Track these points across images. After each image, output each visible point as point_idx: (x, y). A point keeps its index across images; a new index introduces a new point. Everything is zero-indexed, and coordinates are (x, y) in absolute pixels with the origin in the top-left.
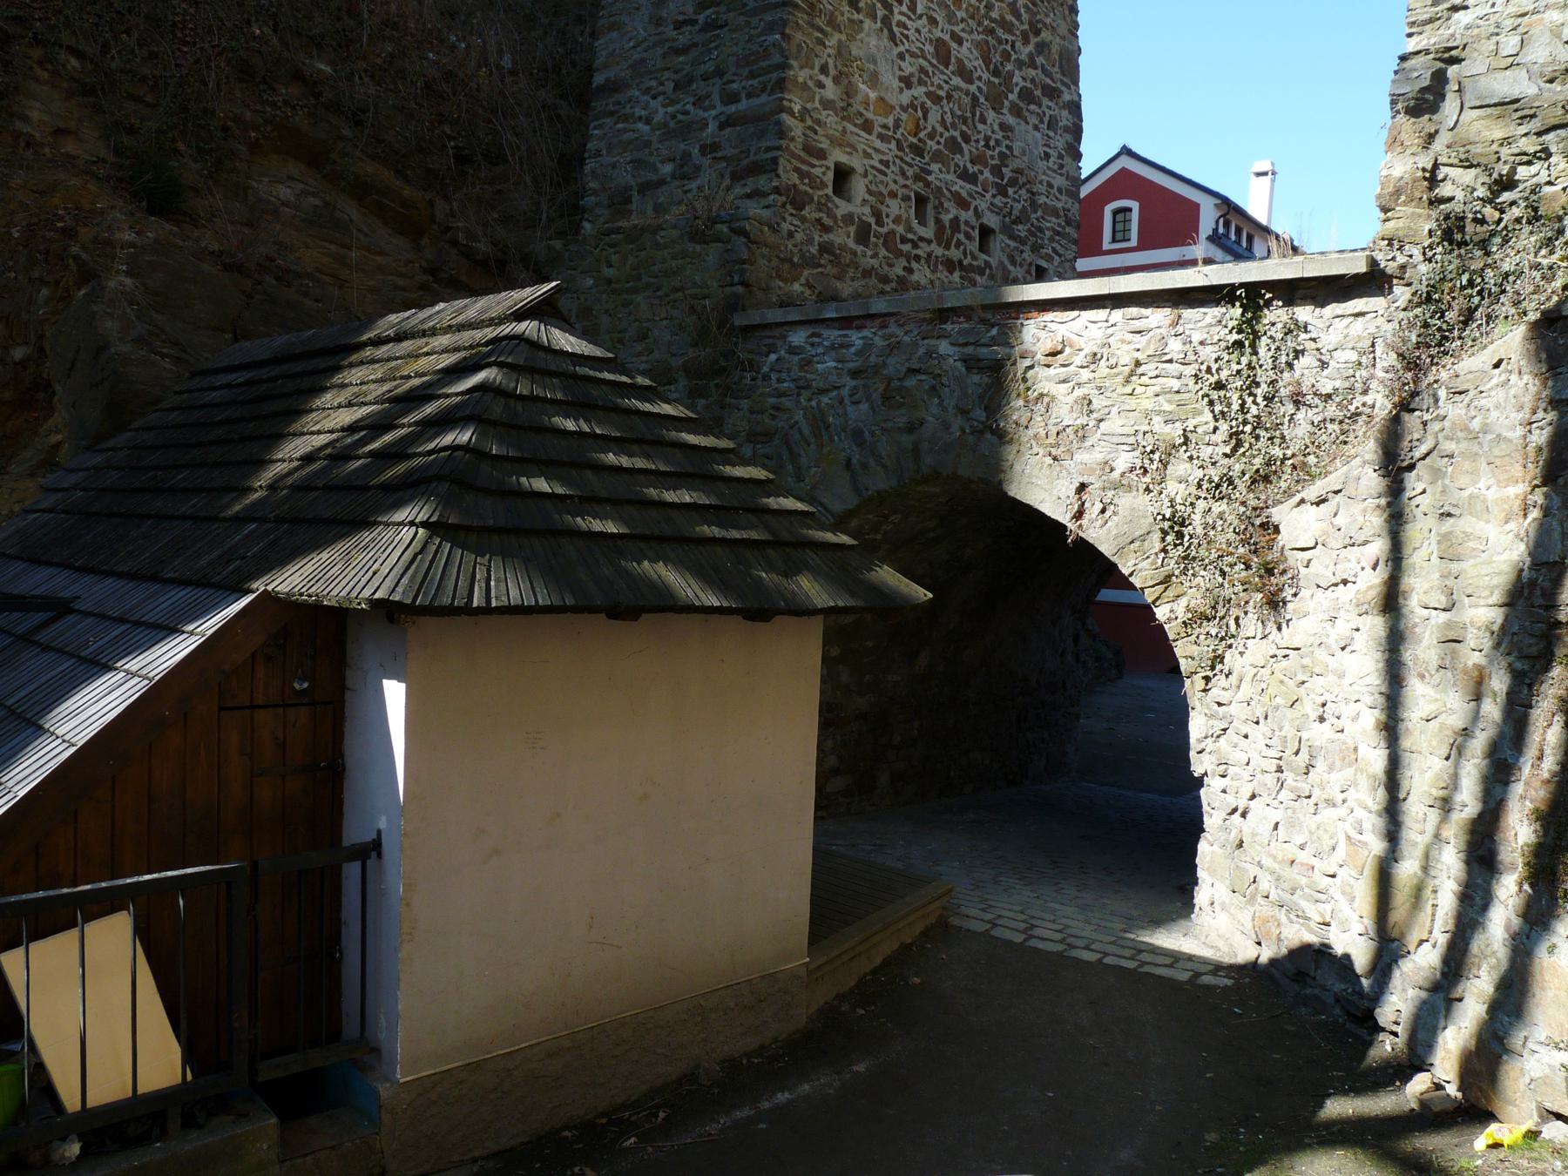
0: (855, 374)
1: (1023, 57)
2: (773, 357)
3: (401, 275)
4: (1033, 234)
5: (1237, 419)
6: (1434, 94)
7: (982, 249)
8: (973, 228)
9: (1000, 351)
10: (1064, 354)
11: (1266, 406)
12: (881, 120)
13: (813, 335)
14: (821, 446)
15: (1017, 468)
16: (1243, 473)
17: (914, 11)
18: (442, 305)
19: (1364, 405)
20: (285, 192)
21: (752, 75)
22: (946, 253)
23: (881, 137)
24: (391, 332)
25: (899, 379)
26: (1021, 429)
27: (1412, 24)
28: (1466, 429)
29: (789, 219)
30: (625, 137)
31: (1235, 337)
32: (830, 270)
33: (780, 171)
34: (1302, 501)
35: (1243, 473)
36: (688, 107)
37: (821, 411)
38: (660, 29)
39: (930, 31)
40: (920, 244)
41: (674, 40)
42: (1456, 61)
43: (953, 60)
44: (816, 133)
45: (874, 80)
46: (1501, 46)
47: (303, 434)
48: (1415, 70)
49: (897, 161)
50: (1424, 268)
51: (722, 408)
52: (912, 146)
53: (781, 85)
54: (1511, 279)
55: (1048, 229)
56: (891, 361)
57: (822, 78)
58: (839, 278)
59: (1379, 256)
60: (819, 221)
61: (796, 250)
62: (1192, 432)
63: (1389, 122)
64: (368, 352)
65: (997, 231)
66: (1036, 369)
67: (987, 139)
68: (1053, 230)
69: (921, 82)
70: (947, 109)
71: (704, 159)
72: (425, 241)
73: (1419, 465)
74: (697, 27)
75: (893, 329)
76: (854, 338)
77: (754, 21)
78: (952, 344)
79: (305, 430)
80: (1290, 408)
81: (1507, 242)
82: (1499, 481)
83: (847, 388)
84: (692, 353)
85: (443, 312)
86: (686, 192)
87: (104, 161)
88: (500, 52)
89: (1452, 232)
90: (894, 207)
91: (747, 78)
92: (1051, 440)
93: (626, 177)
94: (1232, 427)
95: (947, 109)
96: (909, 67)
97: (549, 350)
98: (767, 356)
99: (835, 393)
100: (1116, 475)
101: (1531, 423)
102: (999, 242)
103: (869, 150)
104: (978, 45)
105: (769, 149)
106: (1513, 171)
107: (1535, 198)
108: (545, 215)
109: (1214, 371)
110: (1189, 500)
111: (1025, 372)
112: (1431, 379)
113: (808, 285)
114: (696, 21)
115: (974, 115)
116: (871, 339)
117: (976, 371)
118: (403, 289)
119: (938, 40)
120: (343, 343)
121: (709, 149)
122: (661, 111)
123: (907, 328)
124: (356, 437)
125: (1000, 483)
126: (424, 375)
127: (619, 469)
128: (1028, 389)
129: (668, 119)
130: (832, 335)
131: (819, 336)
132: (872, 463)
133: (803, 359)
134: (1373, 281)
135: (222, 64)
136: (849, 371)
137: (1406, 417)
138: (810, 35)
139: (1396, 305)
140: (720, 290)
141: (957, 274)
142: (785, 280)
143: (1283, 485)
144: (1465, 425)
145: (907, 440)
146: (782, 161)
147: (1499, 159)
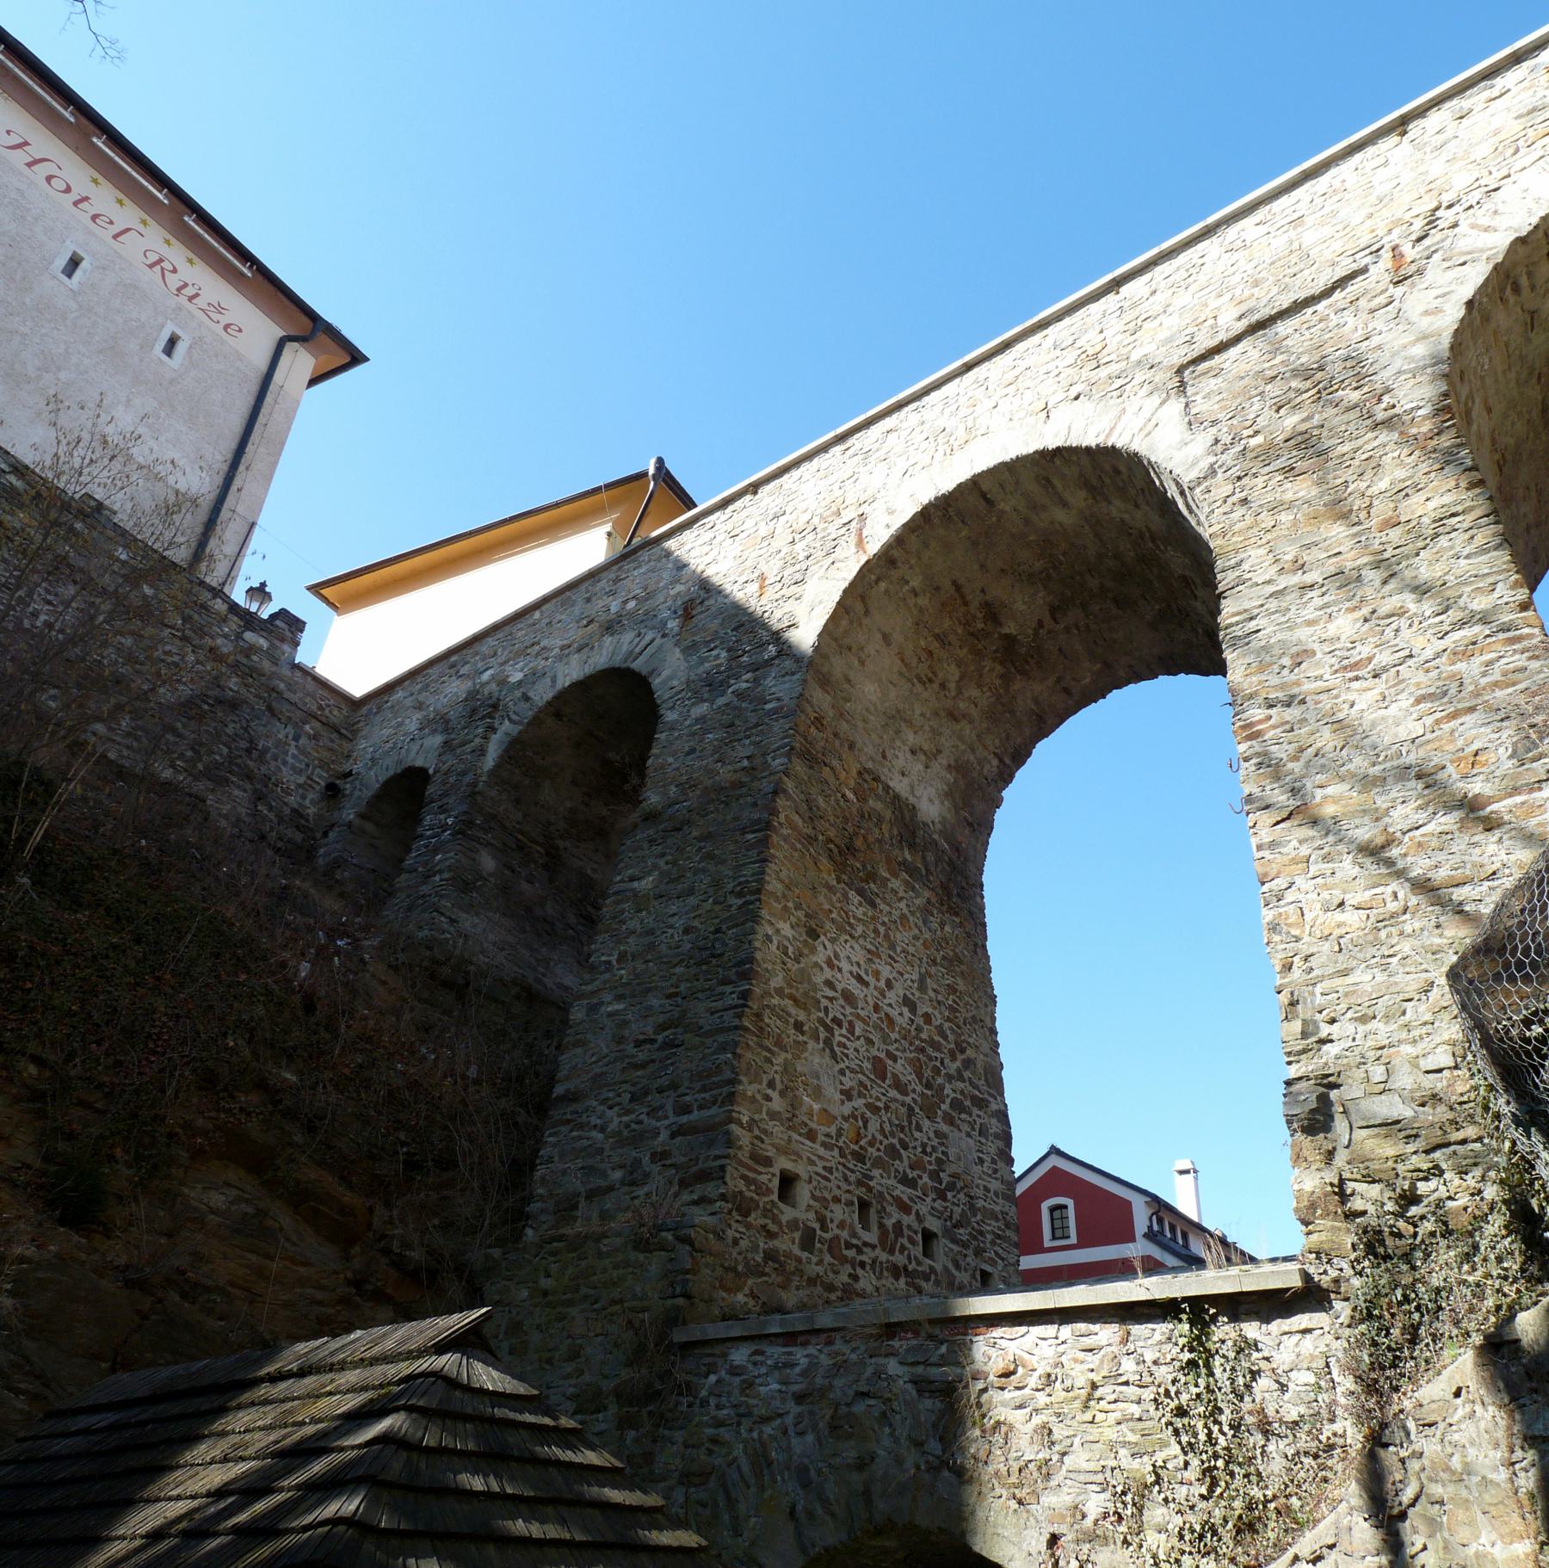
0: (800, 1398)
1: (952, 1072)
2: (713, 1378)
3: (321, 1288)
4: (975, 1238)
5: (1206, 1452)
6: (1323, 1115)
7: (926, 1254)
8: (916, 1233)
9: (949, 1372)
10: (1018, 1375)
11: (1234, 1436)
12: (824, 1129)
13: (756, 1353)
14: (762, 1488)
15: (980, 1514)
16: (1226, 1521)
17: (853, 1033)
18: (359, 1333)
19: (1335, 1435)
20: (218, 1199)
21: (704, 1089)
22: (891, 1258)
23: (825, 1145)
24: (294, 1366)
25: (848, 1405)
26: (980, 1465)
27: (1289, 1054)
28: (1447, 1469)
29: (735, 1225)
30: (579, 1144)
31: (1187, 1356)
32: (775, 1278)
33: (728, 1179)
34: (1296, 1559)
35: (1226, 1521)
36: (642, 1117)
37: (763, 1445)
38: (622, 1047)
39: (867, 1050)
40: (865, 1249)
41: (633, 1056)
42: (1336, 1086)
43: (889, 1075)
44: (762, 1141)
45: (817, 1093)
46: (1371, 1074)
47: (158, 1500)
48: (1302, 1094)
49: (840, 1167)
50: (1356, 1282)
51: (654, 1441)
52: (853, 1153)
53: (731, 1098)
54: (1444, 1294)
55: (988, 1232)
56: (838, 1382)
57: (769, 1092)
58: (784, 1287)
59: (1311, 1270)
60: (764, 1227)
61: (740, 1258)
62: (1161, 1467)
63: (1290, 1140)
64: (263, 1391)
65: (940, 1234)
66: (990, 1392)
67: (924, 1146)
68: (994, 1233)
69: (860, 1095)
70: (885, 1119)
71: (653, 1166)
72: (357, 1249)
73: (1411, 1512)
74: (656, 1046)
75: (839, 1346)
76: (798, 1356)
77: (708, 1041)
78: (901, 1363)
79: (162, 1494)
80: (1259, 1439)
81: (1429, 1256)
82: (1502, 1537)
83: (791, 1416)
84: (625, 1374)
85: (358, 1340)
86: (633, 1198)
87: (29, 1167)
88: (468, 1063)
89: (1373, 1244)
90: (838, 1212)
91: (699, 1092)
92: (1013, 1479)
93: (575, 1184)
94: (1203, 1462)
95: (885, 1119)
96: (849, 1082)
97: (469, 1389)
98: (706, 1377)
99: (778, 1422)
100: (1089, 1522)
101: (1513, 1464)
102: (942, 1246)
103: (814, 1158)
104: (911, 1062)
105: (717, 1158)
106: (1413, 1187)
107: (1442, 1212)
108: (487, 1222)
109: (1173, 1394)
110: (1173, 1555)
111: (979, 1396)
112: (1396, 1408)
113: (753, 1295)
114: (655, 1041)
115: (910, 1123)
116: (817, 1357)
117: (927, 1394)
118: (320, 1303)
119: (875, 1058)
120: (236, 1378)
121: (659, 1156)
122: (616, 1120)
123: (854, 1345)
124: (222, 1505)
125: (963, 1534)
126: (320, 1421)
127: (527, 1541)
128: (984, 1416)
129: (622, 1127)
130: (775, 1352)
131: (762, 1353)
132: (819, 1511)
133: (744, 1381)
134: (1310, 1297)
135: (187, 1073)
136: (794, 1394)
137: (1382, 1453)
138: (758, 1054)
139: (1340, 1321)
140: (661, 1302)
141: (902, 1280)
142: (729, 1291)
143: (1271, 1535)
144: (1445, 1464)
145: (856, 1477)
146: (729, 1168)
147: (1397, 1175)
